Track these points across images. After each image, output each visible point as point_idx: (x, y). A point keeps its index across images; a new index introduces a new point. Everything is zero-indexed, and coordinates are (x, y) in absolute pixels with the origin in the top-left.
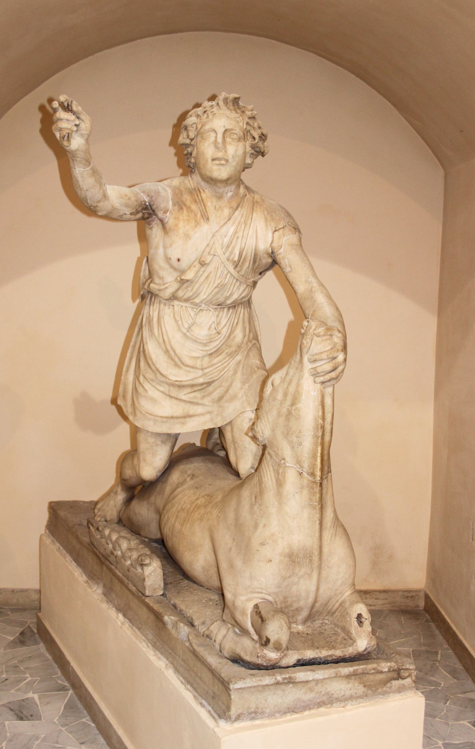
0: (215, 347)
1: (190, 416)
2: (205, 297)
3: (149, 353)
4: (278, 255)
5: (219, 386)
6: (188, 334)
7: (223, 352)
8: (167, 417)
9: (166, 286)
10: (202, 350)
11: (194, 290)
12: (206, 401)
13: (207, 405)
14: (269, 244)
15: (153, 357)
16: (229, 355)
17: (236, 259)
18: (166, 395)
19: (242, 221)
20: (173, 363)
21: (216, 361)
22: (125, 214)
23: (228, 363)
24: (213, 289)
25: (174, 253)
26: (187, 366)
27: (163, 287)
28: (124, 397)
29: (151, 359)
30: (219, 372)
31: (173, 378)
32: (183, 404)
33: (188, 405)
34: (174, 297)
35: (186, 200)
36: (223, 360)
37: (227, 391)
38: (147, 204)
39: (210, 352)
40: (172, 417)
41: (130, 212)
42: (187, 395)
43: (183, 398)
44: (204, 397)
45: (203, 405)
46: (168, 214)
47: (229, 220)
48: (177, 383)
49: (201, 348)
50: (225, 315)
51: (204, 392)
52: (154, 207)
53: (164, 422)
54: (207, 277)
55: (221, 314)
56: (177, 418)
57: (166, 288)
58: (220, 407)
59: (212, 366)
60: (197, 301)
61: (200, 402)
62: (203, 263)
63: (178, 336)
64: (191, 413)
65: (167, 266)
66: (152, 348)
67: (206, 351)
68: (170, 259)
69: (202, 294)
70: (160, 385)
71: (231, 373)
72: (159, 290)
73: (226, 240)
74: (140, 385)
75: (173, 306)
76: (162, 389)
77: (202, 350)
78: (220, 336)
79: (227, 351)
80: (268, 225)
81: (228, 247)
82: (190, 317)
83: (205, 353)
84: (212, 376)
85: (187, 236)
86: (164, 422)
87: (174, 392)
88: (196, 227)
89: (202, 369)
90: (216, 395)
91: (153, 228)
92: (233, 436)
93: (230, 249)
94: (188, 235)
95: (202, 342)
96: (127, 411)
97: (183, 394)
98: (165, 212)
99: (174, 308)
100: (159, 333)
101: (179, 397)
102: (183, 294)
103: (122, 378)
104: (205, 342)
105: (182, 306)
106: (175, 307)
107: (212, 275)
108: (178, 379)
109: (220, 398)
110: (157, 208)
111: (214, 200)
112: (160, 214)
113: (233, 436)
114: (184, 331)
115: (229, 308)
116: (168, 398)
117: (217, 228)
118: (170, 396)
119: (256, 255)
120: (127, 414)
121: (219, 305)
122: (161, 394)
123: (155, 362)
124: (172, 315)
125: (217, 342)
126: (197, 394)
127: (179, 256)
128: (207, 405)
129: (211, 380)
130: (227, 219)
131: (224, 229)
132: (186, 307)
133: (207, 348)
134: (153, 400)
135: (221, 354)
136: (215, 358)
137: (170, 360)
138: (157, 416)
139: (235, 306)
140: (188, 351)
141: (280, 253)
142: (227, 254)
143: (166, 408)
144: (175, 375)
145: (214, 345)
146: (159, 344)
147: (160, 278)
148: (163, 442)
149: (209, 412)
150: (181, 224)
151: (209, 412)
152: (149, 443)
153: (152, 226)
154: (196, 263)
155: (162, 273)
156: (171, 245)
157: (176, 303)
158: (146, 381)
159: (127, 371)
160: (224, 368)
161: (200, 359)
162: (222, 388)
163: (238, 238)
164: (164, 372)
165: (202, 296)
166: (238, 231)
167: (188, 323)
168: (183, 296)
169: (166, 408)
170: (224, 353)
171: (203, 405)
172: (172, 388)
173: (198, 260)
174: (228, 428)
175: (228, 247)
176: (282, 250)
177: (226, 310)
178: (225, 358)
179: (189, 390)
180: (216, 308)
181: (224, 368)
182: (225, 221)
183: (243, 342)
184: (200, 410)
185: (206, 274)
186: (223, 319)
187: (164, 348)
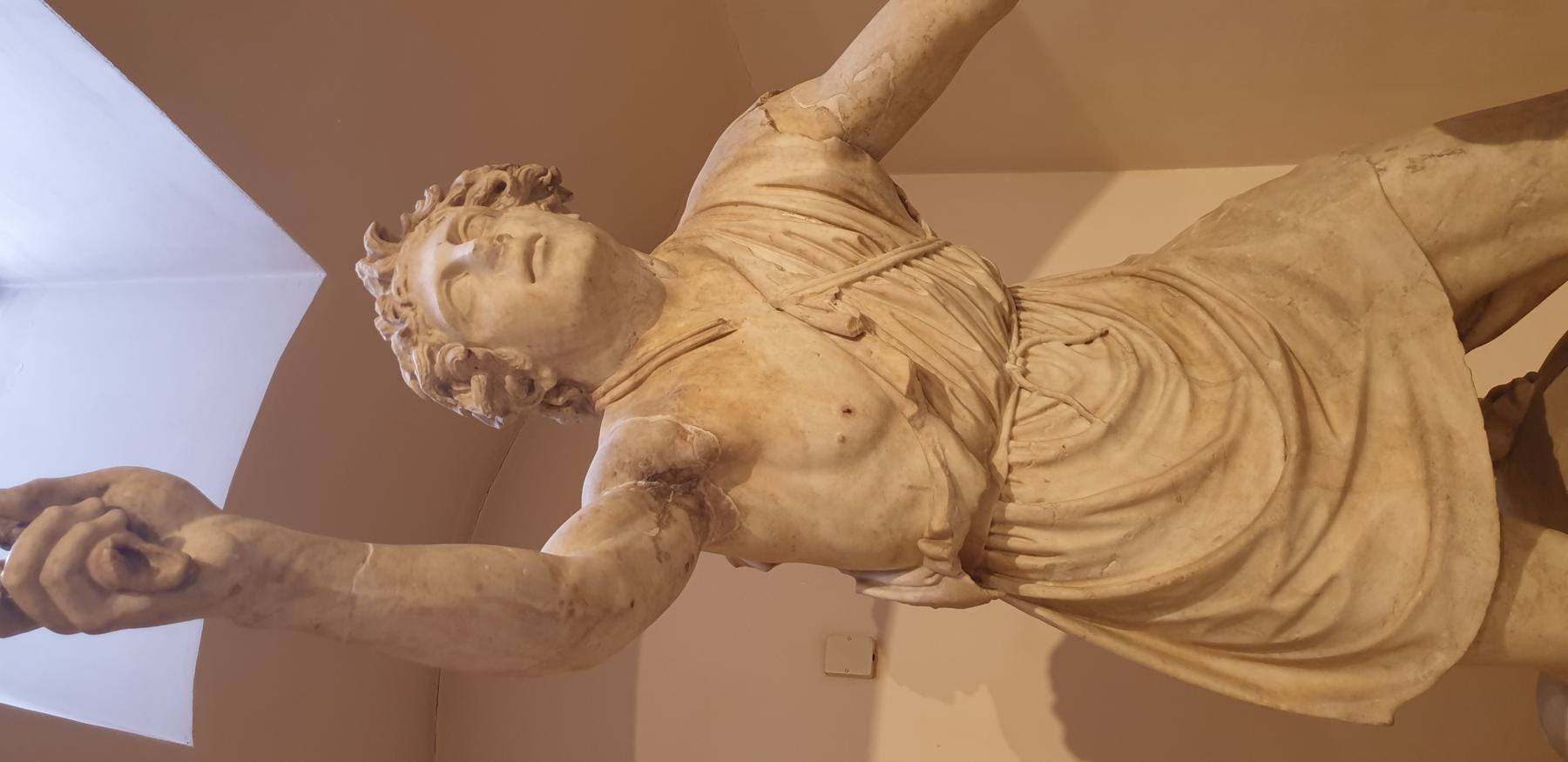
0: (1153, 344)
1: (1416, 412)
2: (979, 349)
3: (1185, 567)
4: (846, 118)
5: (1293, 317)
6: (1110, 418)
7: (1168, 326)
8: (1431, 504)
9: (936, 465)
10: (1166, 383)
11: (957, 377)
12: (1353, 359)
13: (1368, 358)
14: (813, 144)
15: (1198, 551)
16: (1180, 308)
17: (852, 237)
18: (1341, 502)
19: (740, 230)
20: (1216, 474)
21: (1200, 344)
22: (654, 539)
23: (1204, 298)
24: (950, 319)
25: (823, 426)
26: (1226, 425)
27: (943, 479)
28: (1356, 697)
29: (1206, 557)
30: (1241, 320)
31: (1278, 469)
32: (1371, 451)
33: (1372, 430)
34: (982, 450)
35: (662, 390)
36: (1197, 320)
37: (1308, 283)
38: (642, 483)
39: (1172, 357)
40: (1429, 482)
41: (653, 524)
42: (1338, 431)
43: (1347, 437)
44: (1338, 372)
45: (1367, 372)
46: (688, 427)
47: (731, 262)
48: (1294, 449)
49: (1160, 388)
50: (1039, 316)
51: (1321, 374)
52: (661, 468)
53: (1451, 510)
54: (911, 331)
55: (1035, 325)
56: (1427, 464)
57: (945, 466)
58: (1369, 305)
59: (1219, 352)
60: (990, 377)
61: (1356, 377)
62: (857, 327)
63: (1117, 455)
64: (1400, 419)
65: (871, 465)
66: (1159, 563)
67: (1167, 370)
68: (843, 440)
69: (966, 356)
70: (1304, 522)
71: (1242, 280)
72: (955, 493)
73: (792, 265)
74: (1310, 615)
75: (1010, 468)
76: (1320, 516)
77: (1166, 383)
78: (1112, 331)
79: (1165, 316)
80: (754, 150)
81: (814, 262)
82: (1049, 412)
83: (1176, 373)
84: (1258, 339)
85: (772, 379)
86: (1451, 510)
87: (1330, 469)
88: (744, 354)
89: (1235, 377)
90: (1326, 326)
91: (743, 502)
92: (1485, 237)
93: (821, 255)
94: (768, 377)
95: (1135, 376)
96: (1417, 682)
97: (1337, 435)
98: (683, 434)
99: (1022, 465)
100: (1111, 526)
101: (1348, 455)
102: (965, 412)
103: (1283, 706)
104: (1134, 367)
105: (1011, 438)
106: (1013, 458)
107: (901, 315)
108: (1278, 452)
109: (1338, 306)
110: (661, 455)
111: (669, 312)
112: (688, 452)
113: (1485, 237)
114: (1099, 428)
115: (1019, 309)
116: (1351, 499)
117: (756, 299)
118: (1347, 488)
119: (848, 197)
120: (1431, 679)
121: (1009, 330)
122: (1338, 525)
123: (1219, 545)
124: (1043, 473)
125: (1136, 338)
126: (1328, 397)
127: (836, 409)
128: (1368, 358)
129: (1272, 336)
130: (734, 275)
131: (757, 273)
132: (1014, 423)
133: (1159, 368)
134: (1368, 553)
135: (1175, 332)
136: (1192, 349)
137: (1210, 486)
138: (1430, 540)
139: (1016, 298)
140: (1169, 435)
141: (841, 106)
142: (838, 265)
143: (1393, 503)
144: (1266, 460)
145: (1147, 347)
146: (1150, 524)
147: (912, 504)
148: (1528, 545)
149: (1395, 347)
150: (728, 393)
151: (1395, 347)
152: (1539, 596)
153: (733, 507)
154: (858, 349)
155: (896, 490)
156: (797, 434)
157: (1000, 458)
158: (1293, 584)
159: (1258, 689)
160: (1227, 304)
161: (1198, 389)
162: (1301, 306)
163: (788, 233)
164: (1256, 505)
165: (974, 352)
166: (765, 235)
167: (1072, 419)
168: (976, 418)
169: (1393, 503)
170: (1174, 324)
171: (1367, 372)
172: (1315, 476)
173: (849, 345)
174: (1452, 266)
175: (814, 262)
176: (831, 104)
177: (1023, 315)
178: (1192, 316)
179: (1315, 417)
180: (1020, 338)
181: (1227, 304)
182: (738, 278)
183: (1133, 275)
184: (1388, 387)
185: (899, 331)
186: (1056, 323)
187: (1161, 506)
